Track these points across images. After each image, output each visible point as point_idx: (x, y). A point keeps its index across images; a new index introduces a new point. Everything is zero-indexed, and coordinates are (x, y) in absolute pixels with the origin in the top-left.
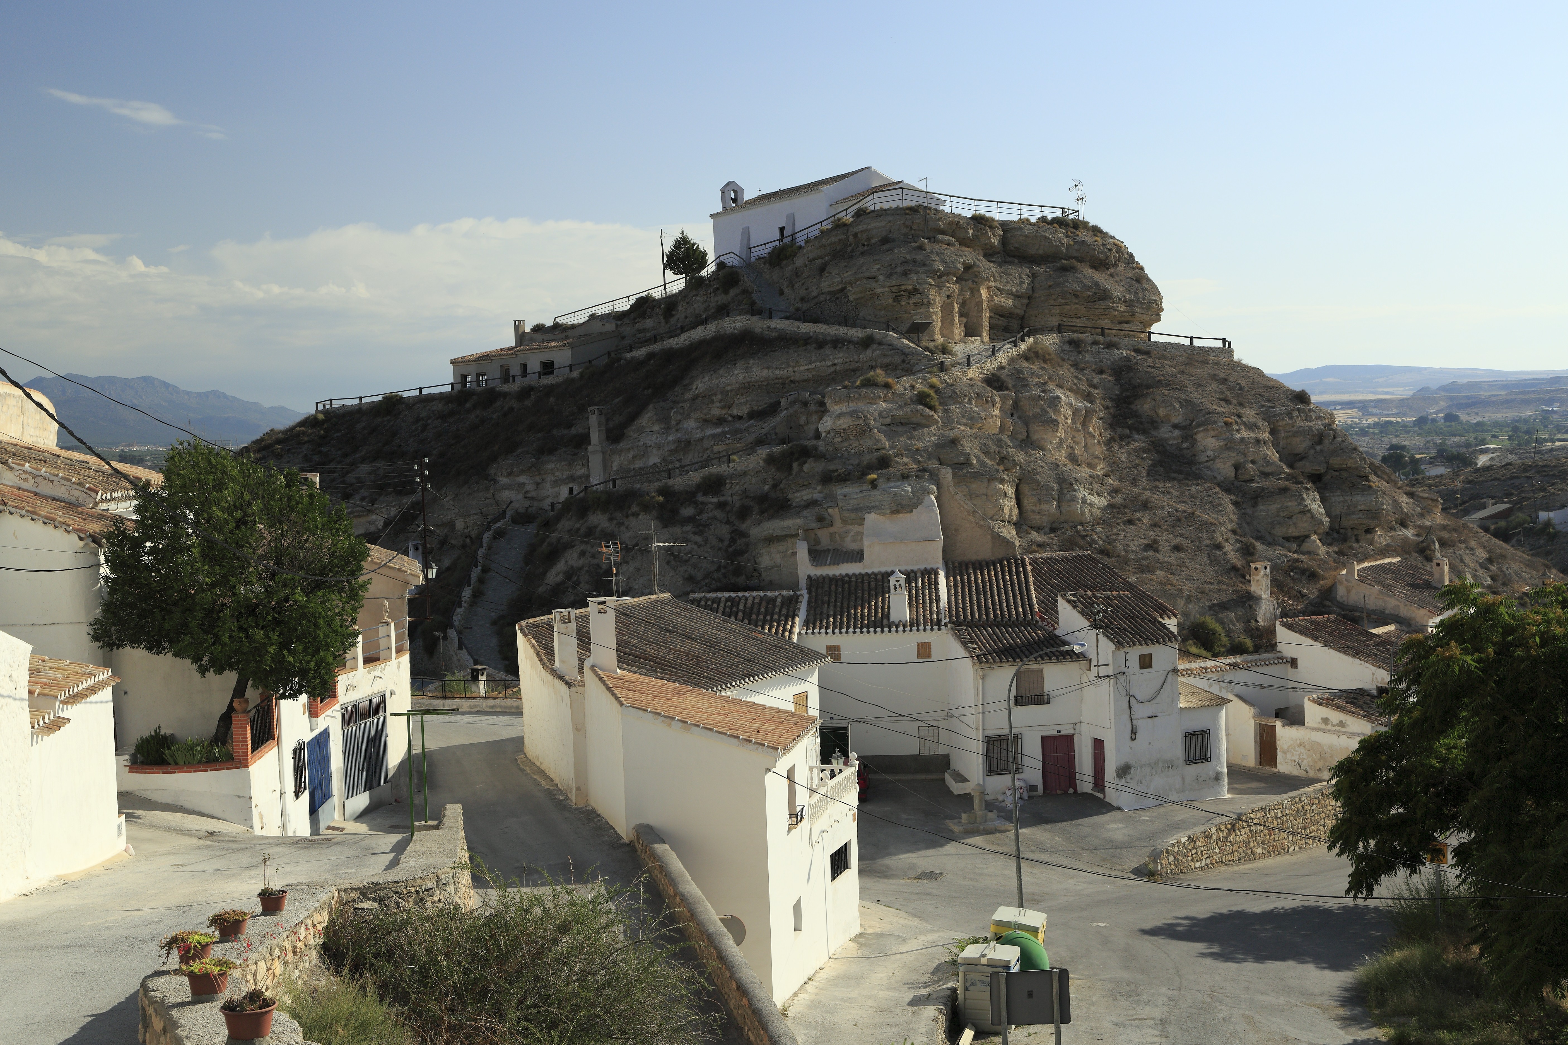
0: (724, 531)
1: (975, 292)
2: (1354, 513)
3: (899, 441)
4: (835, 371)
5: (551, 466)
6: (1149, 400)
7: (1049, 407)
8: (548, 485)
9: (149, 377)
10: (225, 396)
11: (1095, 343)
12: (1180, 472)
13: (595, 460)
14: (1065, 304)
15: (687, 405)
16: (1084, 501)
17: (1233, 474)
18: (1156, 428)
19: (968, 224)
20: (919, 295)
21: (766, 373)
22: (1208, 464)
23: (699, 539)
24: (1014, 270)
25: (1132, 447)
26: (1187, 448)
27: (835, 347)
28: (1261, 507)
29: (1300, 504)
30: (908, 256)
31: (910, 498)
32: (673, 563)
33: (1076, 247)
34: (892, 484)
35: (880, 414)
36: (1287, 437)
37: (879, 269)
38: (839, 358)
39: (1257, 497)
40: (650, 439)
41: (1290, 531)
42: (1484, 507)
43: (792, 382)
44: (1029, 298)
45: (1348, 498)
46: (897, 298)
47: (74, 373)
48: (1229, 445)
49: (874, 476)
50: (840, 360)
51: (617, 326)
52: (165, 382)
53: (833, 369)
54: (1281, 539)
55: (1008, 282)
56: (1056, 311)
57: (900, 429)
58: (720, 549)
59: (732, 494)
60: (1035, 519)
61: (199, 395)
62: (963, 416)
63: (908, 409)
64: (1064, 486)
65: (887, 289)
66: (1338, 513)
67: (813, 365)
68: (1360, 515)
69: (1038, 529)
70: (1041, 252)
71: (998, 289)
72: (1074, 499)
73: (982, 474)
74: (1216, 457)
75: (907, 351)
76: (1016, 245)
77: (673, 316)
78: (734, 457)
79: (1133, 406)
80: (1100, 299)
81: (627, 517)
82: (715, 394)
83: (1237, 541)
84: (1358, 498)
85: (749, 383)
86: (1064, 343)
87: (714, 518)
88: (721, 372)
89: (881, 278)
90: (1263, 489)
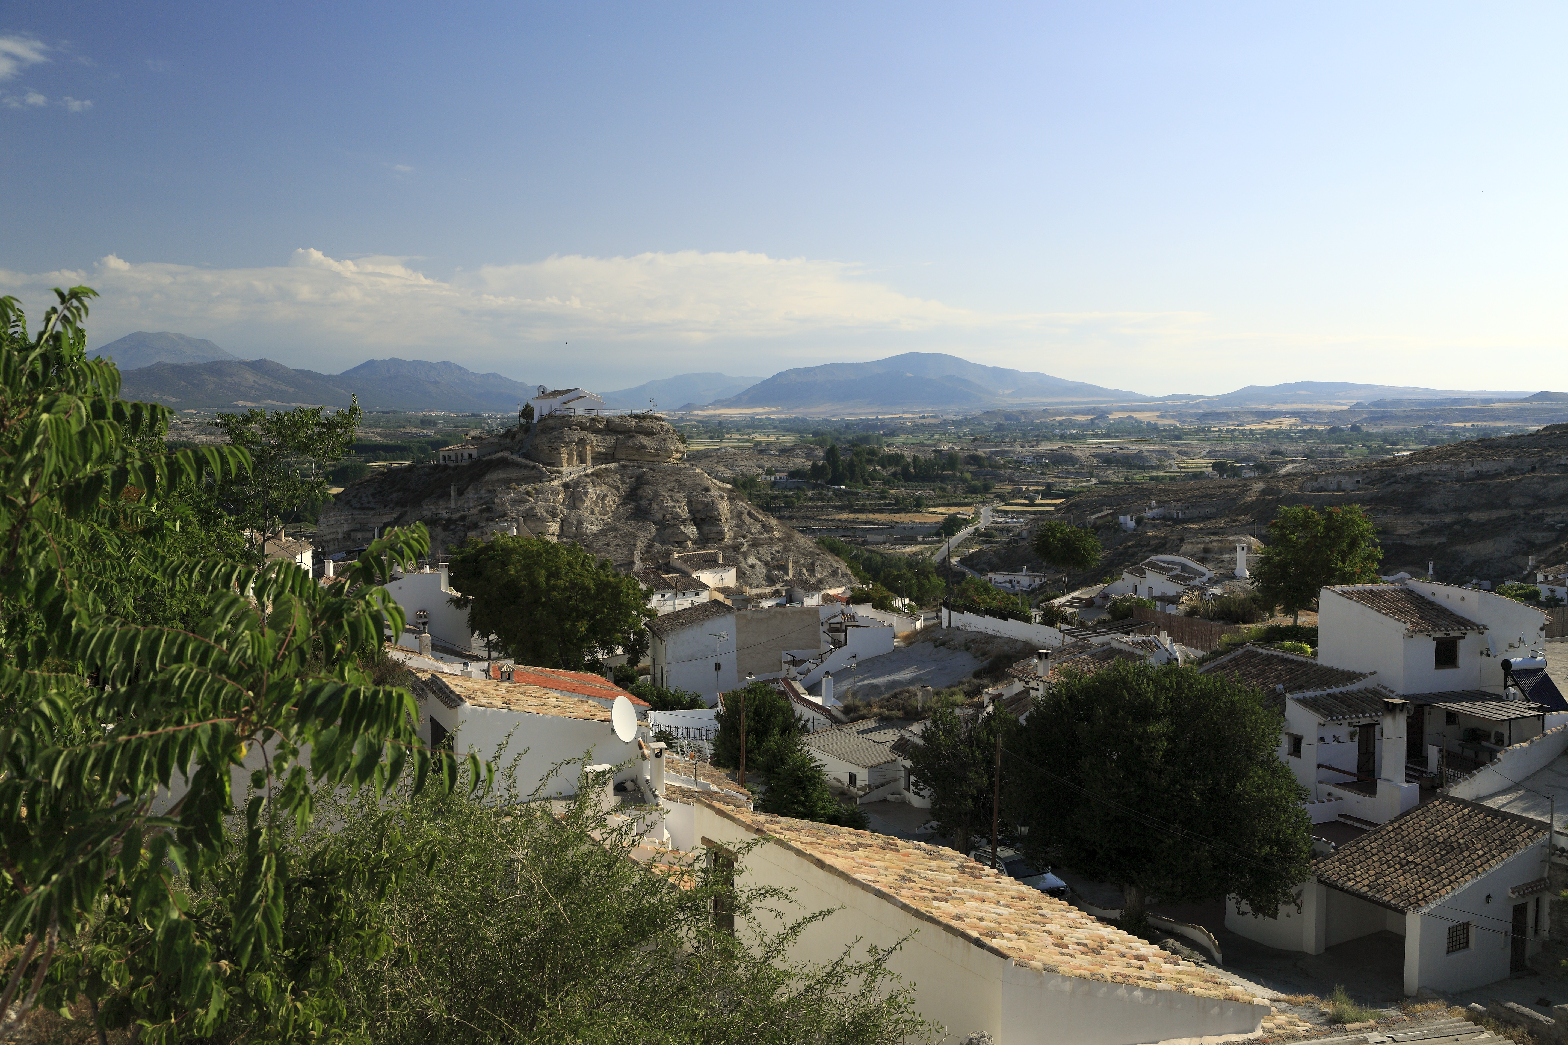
0: (462, 534)
1: (584, 448)
10: (500, 377)
13: (453, 502)
24: (608, 438)
38: (525, 472)
39: (666, 527)
40: (470, 496)
42: (1102, 511)
48: (662, 508)
59: (468, 520)
61: (482, 375)
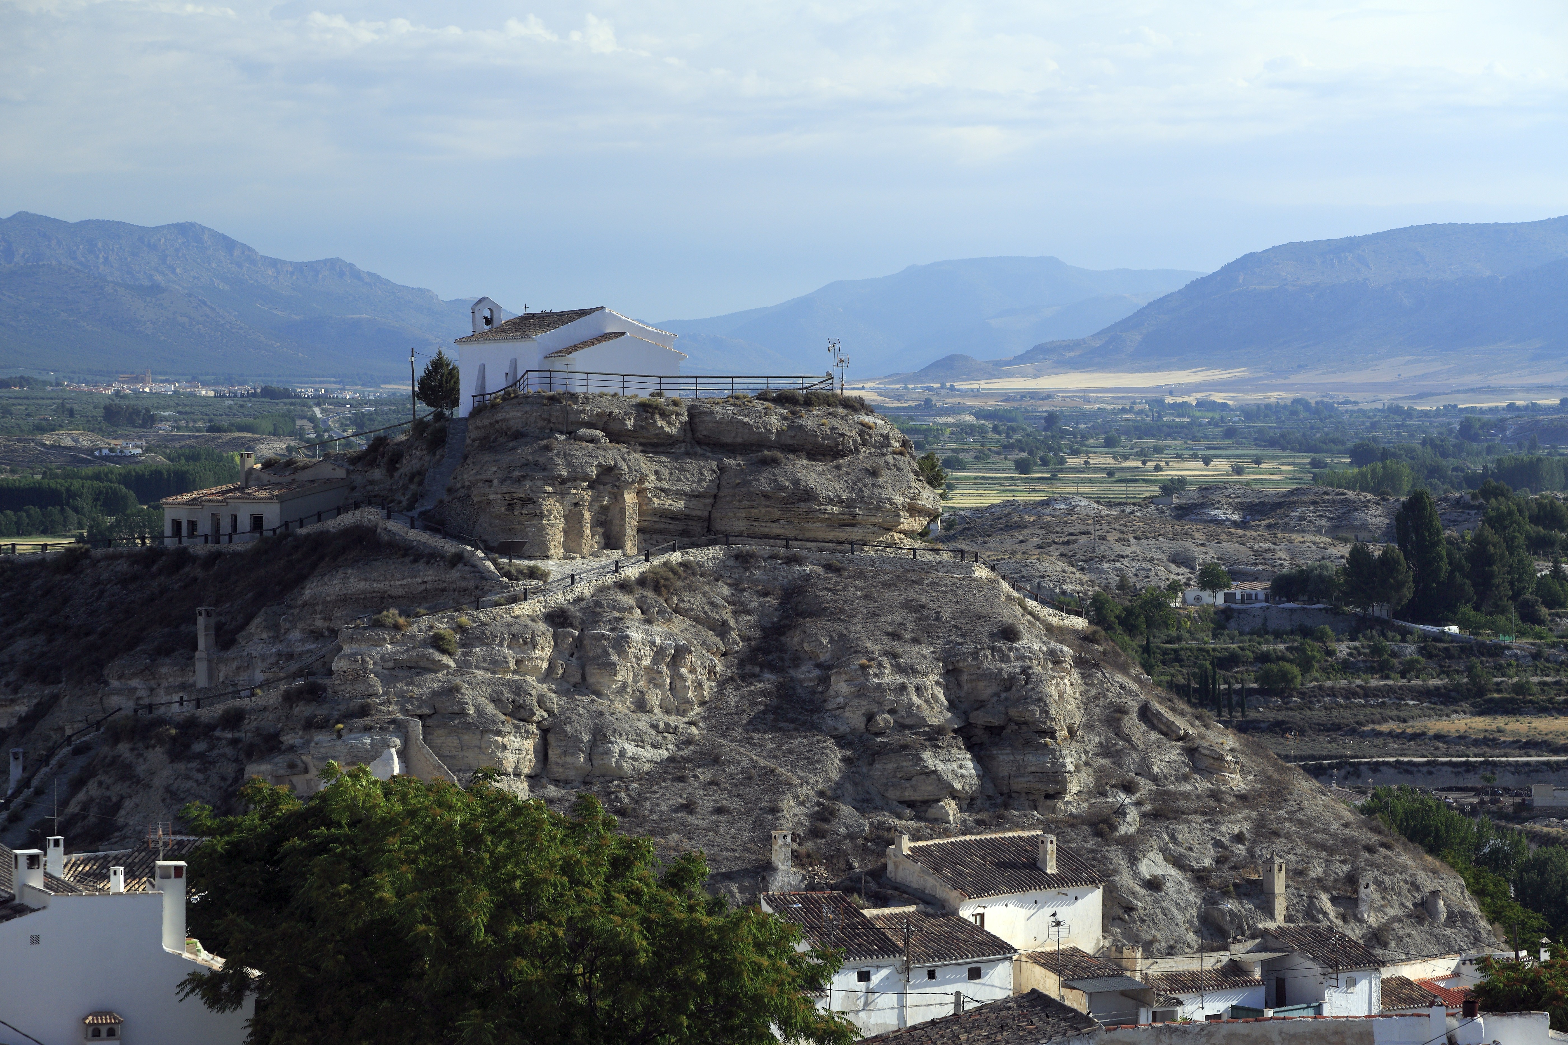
0: (229, 769)
1: (617, 497)
2: (1023, 776)
3: (395, 687)
4: (426, 590)
5: (164, 670)
6: (798, 632)
7: (613, 648)
8: (162, 692)
9: (193, 225)
10: (356, 274)
11: (773, 557)
12: (793, 721)
13: (201, 667)
14: (751, 507)
15: (296, 611)
16: (622, 753)
17: (863, 725)
18: (797, 666)
19: (626, 414)
20: (531, 506)
21: (363, 585)
22: (837, 712)
23: (200, 777)
24: (693, 465)
25: (753, 688)
26: (821, 693)
27: (428, 563)
28: (878, 766)
29: (917, 764)
30: (530, 458)
31: (367, 750)
32: (168, 801)
33: (790, 433)
34: (353, 736)
35: (382, 658)
36: (971, 681)
37: (495, 472)
38: (429, 575)
39: (875, 754)
41: (907, 794)
43: (390, 597)
44: (715, 496)
45: (1019, 757)
46: (510, 506)
47: (31, 211)
48: (862, 692)
49: (341, 726)
50: (430, 578)
51: (348, 472)
52: (224, 237)
53: (423, 587)
54: (895, 803)
55: (680, 480)
56: (742, 514)
57: (401, 674)
58: (220, 788)
60: (559, 772)
61: (300, 267)
62: (485, 660)
63: (413, 653)
64: (598, 737)
65: (499, 496)
66: (1006, 773)
67: (405, 582)
68: (1031, 778)
69: (557, 782)
70: (739, 440)
71: (662, 490)
72: (608, 752)
73: (476, 726)
74: (846, 704)
75: (487, 574)
76: (705, 433)
77: (397, 469)
78: (258, 691)
79: (783, 639)
80: (800, 500)
81: (147, 748)
82: (318, 604)
83: (818, 804)
84: (1030, 758)
85: (345, 595)
86: (728, 558)
87: (224, 755)
88: (326, 579)
89: (496, 482)
90: (887, 744)
